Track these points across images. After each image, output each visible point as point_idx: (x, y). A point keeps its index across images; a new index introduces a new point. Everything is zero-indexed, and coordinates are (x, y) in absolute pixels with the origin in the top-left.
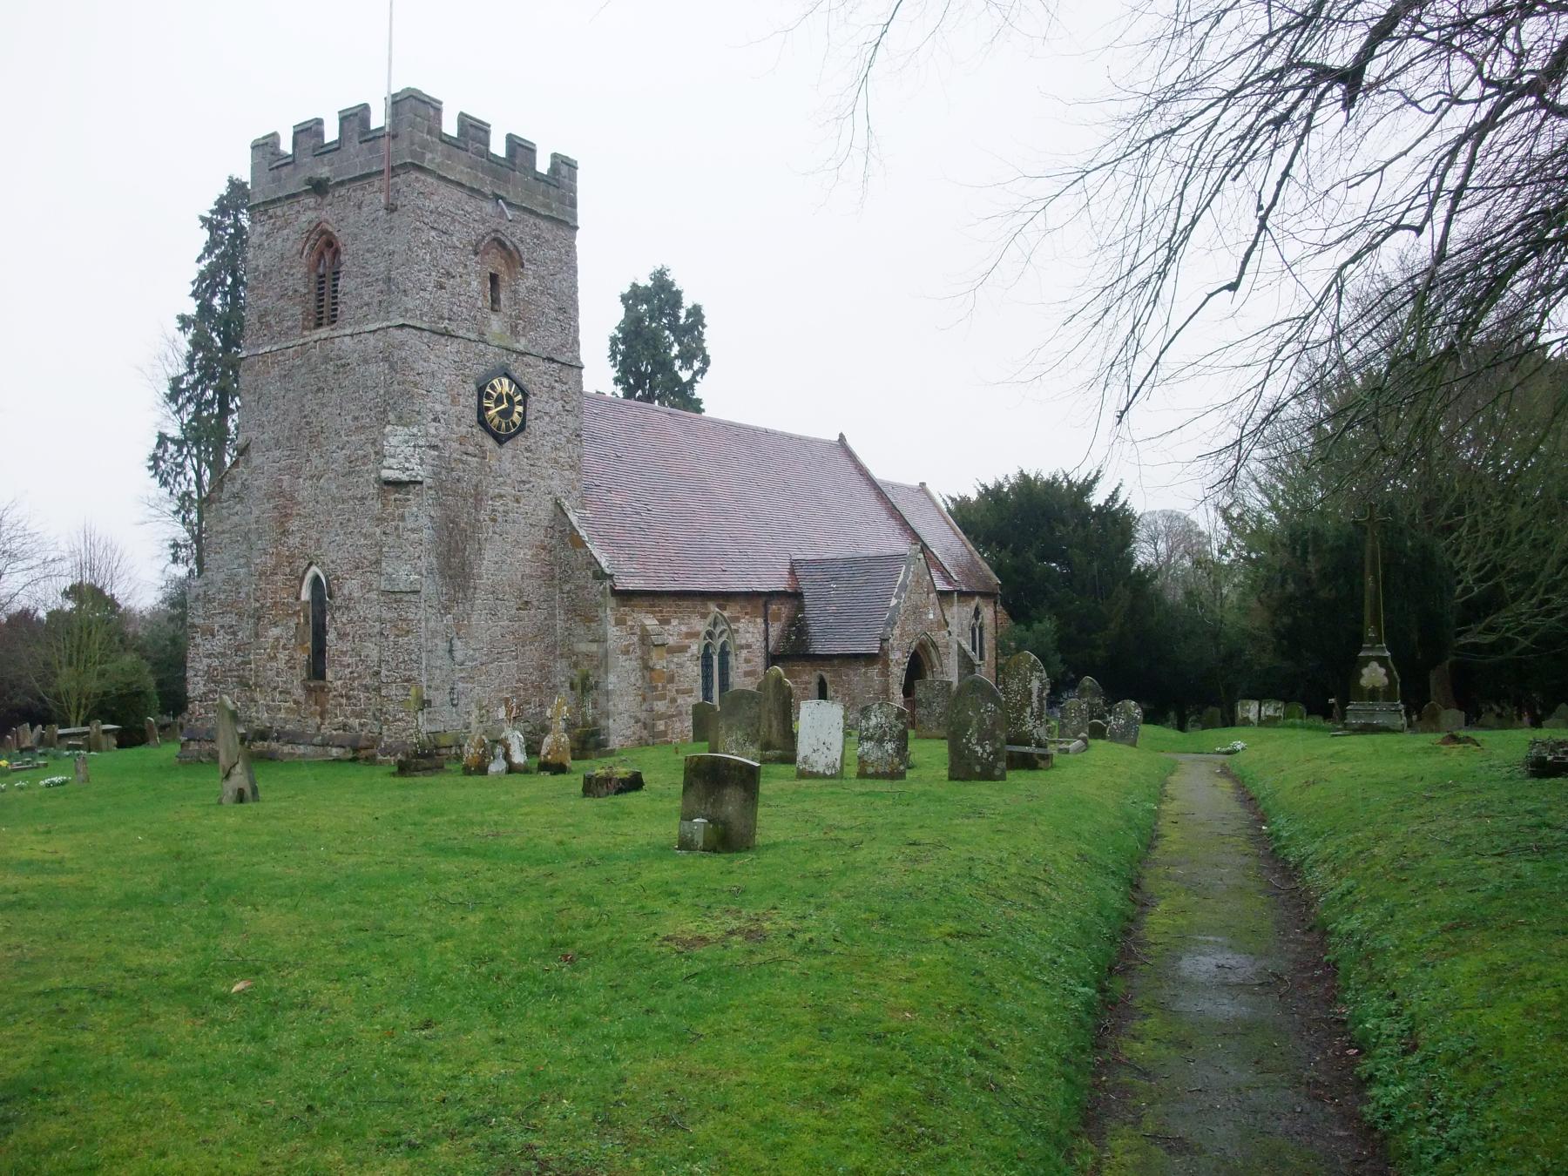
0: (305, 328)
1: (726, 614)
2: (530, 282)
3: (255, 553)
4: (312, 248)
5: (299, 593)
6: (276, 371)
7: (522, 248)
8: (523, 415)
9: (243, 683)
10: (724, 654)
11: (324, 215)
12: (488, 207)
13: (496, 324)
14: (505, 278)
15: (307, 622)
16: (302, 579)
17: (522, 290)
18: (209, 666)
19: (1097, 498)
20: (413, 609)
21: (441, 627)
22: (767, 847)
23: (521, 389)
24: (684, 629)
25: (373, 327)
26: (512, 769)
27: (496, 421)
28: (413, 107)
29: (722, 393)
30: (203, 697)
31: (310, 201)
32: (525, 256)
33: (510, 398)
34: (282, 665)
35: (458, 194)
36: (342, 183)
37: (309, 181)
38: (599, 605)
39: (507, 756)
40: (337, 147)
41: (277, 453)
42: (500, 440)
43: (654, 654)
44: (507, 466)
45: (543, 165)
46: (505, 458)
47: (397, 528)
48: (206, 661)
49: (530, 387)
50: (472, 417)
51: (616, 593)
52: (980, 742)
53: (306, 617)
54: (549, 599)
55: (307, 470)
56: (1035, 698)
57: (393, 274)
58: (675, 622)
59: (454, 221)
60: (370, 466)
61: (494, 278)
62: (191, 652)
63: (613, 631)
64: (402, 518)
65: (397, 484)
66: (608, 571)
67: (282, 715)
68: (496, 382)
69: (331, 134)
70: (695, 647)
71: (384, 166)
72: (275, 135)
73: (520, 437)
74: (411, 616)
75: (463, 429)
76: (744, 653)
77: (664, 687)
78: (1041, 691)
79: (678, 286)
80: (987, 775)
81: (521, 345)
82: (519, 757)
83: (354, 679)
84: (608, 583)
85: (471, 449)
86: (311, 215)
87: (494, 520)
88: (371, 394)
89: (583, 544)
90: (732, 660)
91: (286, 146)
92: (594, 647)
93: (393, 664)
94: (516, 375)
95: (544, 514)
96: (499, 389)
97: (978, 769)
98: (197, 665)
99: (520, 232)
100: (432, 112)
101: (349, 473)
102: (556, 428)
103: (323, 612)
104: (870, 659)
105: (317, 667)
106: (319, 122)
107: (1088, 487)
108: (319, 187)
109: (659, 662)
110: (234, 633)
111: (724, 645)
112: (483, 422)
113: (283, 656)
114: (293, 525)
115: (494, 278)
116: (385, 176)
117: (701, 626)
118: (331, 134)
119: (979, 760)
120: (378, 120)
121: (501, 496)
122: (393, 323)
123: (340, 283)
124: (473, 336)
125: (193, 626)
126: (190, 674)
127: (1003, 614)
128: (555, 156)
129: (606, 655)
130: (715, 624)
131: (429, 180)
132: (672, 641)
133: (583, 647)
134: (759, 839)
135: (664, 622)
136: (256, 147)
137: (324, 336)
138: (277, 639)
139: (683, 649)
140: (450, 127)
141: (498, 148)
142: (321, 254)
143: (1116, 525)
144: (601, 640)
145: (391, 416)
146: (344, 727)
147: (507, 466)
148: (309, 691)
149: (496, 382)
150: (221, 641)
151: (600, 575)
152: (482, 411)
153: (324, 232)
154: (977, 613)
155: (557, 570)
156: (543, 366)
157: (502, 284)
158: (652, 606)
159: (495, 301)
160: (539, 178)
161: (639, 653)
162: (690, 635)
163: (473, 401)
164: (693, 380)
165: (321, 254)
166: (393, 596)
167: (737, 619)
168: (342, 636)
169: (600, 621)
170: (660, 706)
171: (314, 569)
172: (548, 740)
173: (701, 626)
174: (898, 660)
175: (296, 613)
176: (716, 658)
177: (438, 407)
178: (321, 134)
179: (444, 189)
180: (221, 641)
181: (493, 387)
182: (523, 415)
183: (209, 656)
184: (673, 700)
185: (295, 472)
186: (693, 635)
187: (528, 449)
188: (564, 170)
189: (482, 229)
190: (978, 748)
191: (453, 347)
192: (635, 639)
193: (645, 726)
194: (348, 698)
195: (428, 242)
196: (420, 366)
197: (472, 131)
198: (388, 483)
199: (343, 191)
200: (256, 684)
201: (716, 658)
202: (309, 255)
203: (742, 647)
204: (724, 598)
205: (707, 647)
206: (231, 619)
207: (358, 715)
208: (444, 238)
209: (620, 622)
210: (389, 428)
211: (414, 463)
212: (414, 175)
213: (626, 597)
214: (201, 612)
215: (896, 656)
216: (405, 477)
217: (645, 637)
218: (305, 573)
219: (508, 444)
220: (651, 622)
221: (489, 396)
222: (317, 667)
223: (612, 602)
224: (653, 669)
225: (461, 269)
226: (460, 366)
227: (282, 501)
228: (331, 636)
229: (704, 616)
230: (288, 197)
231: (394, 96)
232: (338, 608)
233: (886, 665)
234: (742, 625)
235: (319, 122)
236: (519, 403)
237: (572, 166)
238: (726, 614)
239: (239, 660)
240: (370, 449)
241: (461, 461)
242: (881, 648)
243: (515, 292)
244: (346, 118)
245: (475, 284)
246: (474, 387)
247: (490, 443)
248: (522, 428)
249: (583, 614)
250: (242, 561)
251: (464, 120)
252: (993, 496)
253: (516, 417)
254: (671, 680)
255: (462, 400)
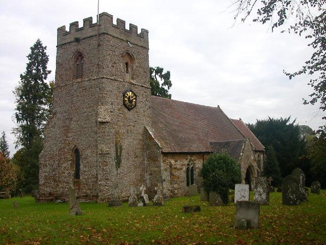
2: (137, 64)
8: (135, 102)
9: (55, 181)
11: (79, 47)
12: (125, 44)
17: (135, 67)
19: (290, 122)
20: (108, 159)
23: (135, 95)
28: (105, 17)
29: (172, 98)
31: (75, 44)
34: (66, 174)
35: (117, 41)
42: (129, 109)
45: (139, 32)
46: (130, 114)
51: (163, 153)
52: (292, 195)
54: (143, 155)
58: (179, 161)
63: (162, 164)
64: (104, 132)
69: (81, 25)
70: (184, 169)
72: (64, 26)
75: (119, 107)
78: (303, 179)
80: (295, 203)
86: (75, 47)
91: (68, 29)
92: (157, 169)
97: (291, 202)
100: (110, 19)
103: (79, 160)
105: (77, 175)
107: (286, 121)
108: (77, 40)
112: (125, 104)
115: (127, 64)
117: (186, 162)
118: (81, 25)
119: (292, 200)
123: (84, 66)
124: (122, 80)
131: (110, 37)
132: (178, 167)
136: (59, 29)
141: (127, 27)
151: (159, 148)
152: (124, 101)
153: (79, 52)
154: (259, 156)
156: (140, 88)
159: (127, 70)
162: (183, 165)
163: (122, 99)
165: (78, 59)
166: (103, 155)
167: (195, 160)
169: (157, 160)
170: (176, 186)
172: (156, 196)
173: (186, 162)
178: (78, 26)
181: (127, 94)
182: (135, 102)
188: (145, 33)
191: (116, 84)
194: (87, 184)
197: (121, 24)
198: (100, 122)
204: (192, 154)
207: (90, 189)
209: (164, 161)
213: (166, 154)
216: (104, 121)
217: (171, 166)
220: (173, 162)
221: (126, 97)
222: (77, 175)
227: (66, 128)
228: (81, 166)
229: (187, 159)
235: (91, 18)
236: (134, 99)
237: (147, 32)
244: (85, 21)
246: (122, 94)
247: (126, 110)
249: (153, 159)
252: (260, 124)
254: (178, 178)
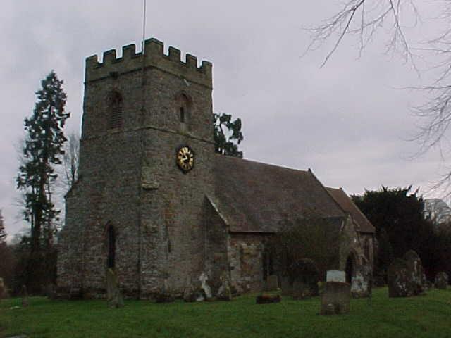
8: (193, 162)
14: (186, 110)
17: (192, 114)
23: (192, 152)
27: (183, 164)
28: (153, 45)
31: (111, 80)
33: (187, 155)
37: (111, 73)
42: (185, 172)
43: (245, 257)
45: (199, 65)
49: (196, 151)
51: (230, 233)
52: (401, 284)
56: (415, 268)
61: (182, 109)
65: (149, 190)
66: (228, 224)
68: (183, 149)
69: (119, 55)
79: (24, 133)
91: (100, 60)
92: (221, 255)
94: (190, 146)
95: (200, 200)
98: (61, 262)
107: (405, 191)
108: (114, 76)
115: (182, 109)
116: (142, 71)
118: (119, 55)
121: (185, 194)
126: (58, 265)
135: (249, 244)
137: (116, 132)
143: (416, 205)
144: (226, 251)
150: (71, 252)
151: (225, 226)
154: (366, 240)
158: (244, 238)
159: (182, 117)
161: (239, 257)
163: (175, 157)
172: (221, 289)
188: (208, 67)
189: (178, 90)
190: (401, 286)
191: (167, 136)
196: (156, 143)
209: (232, 244)
210: (144, 168)
213: (234, 234)
216: (150, 187)
217: (242, 250)
219: (188, 174)
220: (244, 245)
228: (118, 250)
231: (146, 41)
232: (121, 239)
247: (180, 173)
248: (193, 167)
249: (216, 240)
250: (80, 220)
252: (370, 195)
253: (190, 163)
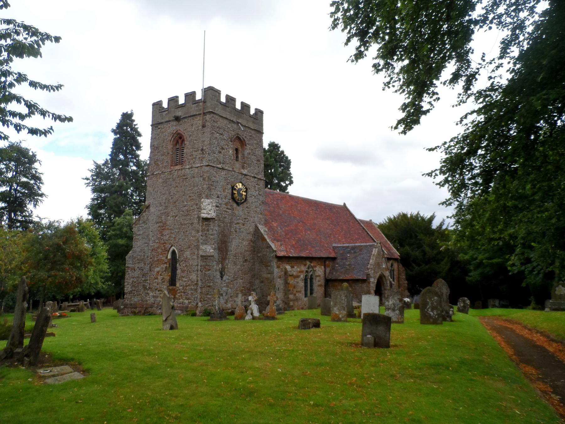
0: (171, 166)
1: (312, 265)
3: (151, 242)
4: (174, 139)
5: (167, 256)
6: (160, 180)
7: (246, 140)
10: (311, 279)
12: (235, 126)
13: (238, 165)
14: (240, 149)
15: (170, 266)
16: (169, 251)
18: (133, 281)
21: (218, 268)
22: (396, 346)
24: (299, 270)
25: (197, 166)
26: (254, 318)
28: (211, 93)
30: (131, 292)
31: (175, 123)
32: (247, 142)
35: (226, 122)
36: (185, 118)
38: (272, 261)
39: (252, 314)
40: (182, 106)
41: (161, 208)
42: (238, 204)
43: (289, 278)
44: (241, 213)
45: (252, 112)
46: (239, 211)
47: (206, 234)
48: (132, 279)
50: (230, 197)
52: (432, 311)
53: (169, 264)
54: (253, 259)
55: (172, 214)
57: (204, 148)
58: (296, 267)
59: (224, 130)
60: (195, 213)
62: (127, 276)
63: (276, 270)
64: (208, 230)
65: (206, 219)
66: (275, 249)
67: (159, 299)
68: (237, 185)
69: (182, 101)
70: (302, 276)
71: (201, 112)
73: (245, 203)
74: (210, 264)
75: (227, 200)
76: (318, 278)
77: (293, 290)
81: (245, 172)
82: (256, 314)
83: (187, 286)
84: (274, 254)
85: (229, 207)
87: (236, 231)
88: (196, 188)
89: (266, 240)
90: (314, 281)
92: (269, 276)
93: (204, 281)
95: (252, 230)
96: (238, 187)
99: (245, 135)
100: (217, 94)
101: (187, 215)
102: (256, 200)
104: (363, 281)
105: (173, 282)
106: (177, 97)
108: (177, 119)
109: (291, 281)
110: (142, 270)
111: (311, 275)
112: (233, 199)
113: (160, 277)
114: (166, 232)
115: (237, 150)
117: (304, 268)
118: (182, 101)
120: (199, 97)
122: (204, 164)
124: (231, 169)
125: (128, 267)
126: (126, 284)
127: (401, 266)
128: (256, 109)
129: (274, 279)
130: (308, 268)
131: (217, 117)
132: (295, 274)
133: (265, 275)
134: (391, 343)
135: (292, 267)
138: (158, 272)
139: (298, 277)
140: (223, 99)
141: (238, 106)
142: (177, 142)
144: (271, 273)
145: (203, 196)
146: (182, 303)
147: (241, 213)
148: (170, 291)
149: (237, 185)
152: (233, 194)
153: (179, 134)
154: (392, 265)
155: (256, 249)
156: (252, 179)
157: (239, 152)
159: (237, 157)
160: (250, 116)
162: (301, 272)
163: (230, 191)
164: (287, 186)
165: (177, 142)
167: (316, 267)
168: (183, 271)
171: (173, 248)
174: (373, 281)
175: (166, 263)
176: (309, 280)
177: (219, 193)
178: (177, 101)
179: (221, 120)
180: (137, 273)
181: (237, 186)
183: (133, 278)
184: (295, 295)
185: (167, 215)
186: (301, 272)
187: (247, 208)
189: (233, 133)
190: (432, 313)
191: (223, 173)
192: (283, 273)
193: (286, 303)
194: (184, 293)
195: (216, 138)
198: (203, 218)
199: (186, 120)
200: (149, 288)
201: (309, 280)
202: (173, 141)
203: (317, 276)
204: (311, 259)
205: (306, 276)
206: (142, 265)
208: (221, 136)
211: (212, 212)
212: (212, 115)
214: (131, 262)
215: (372, 280)
216: (209, 216)
217: (286, 272)
218: (170, 249)
220: (288, 267)
221: (235, 189)
223: (276, 260)
224: (289, 284)
225: (226, 147)
226: (226, 179)
228: (179, 271)
229: (305, 265)
230: (166, 122)
233: (369, 283)
234: (317, 268)
235: (177, 97)
237: (262, 112)
238: (312, 265)
239: (143, 279)
240: (195, 207)
241: (226, 211)
242: (367, 277)
243: (243, 154)
244: (187, 95)
245: (231, 152)
247: (235, 205)
251: (228, 97)
255: (226, 191)
